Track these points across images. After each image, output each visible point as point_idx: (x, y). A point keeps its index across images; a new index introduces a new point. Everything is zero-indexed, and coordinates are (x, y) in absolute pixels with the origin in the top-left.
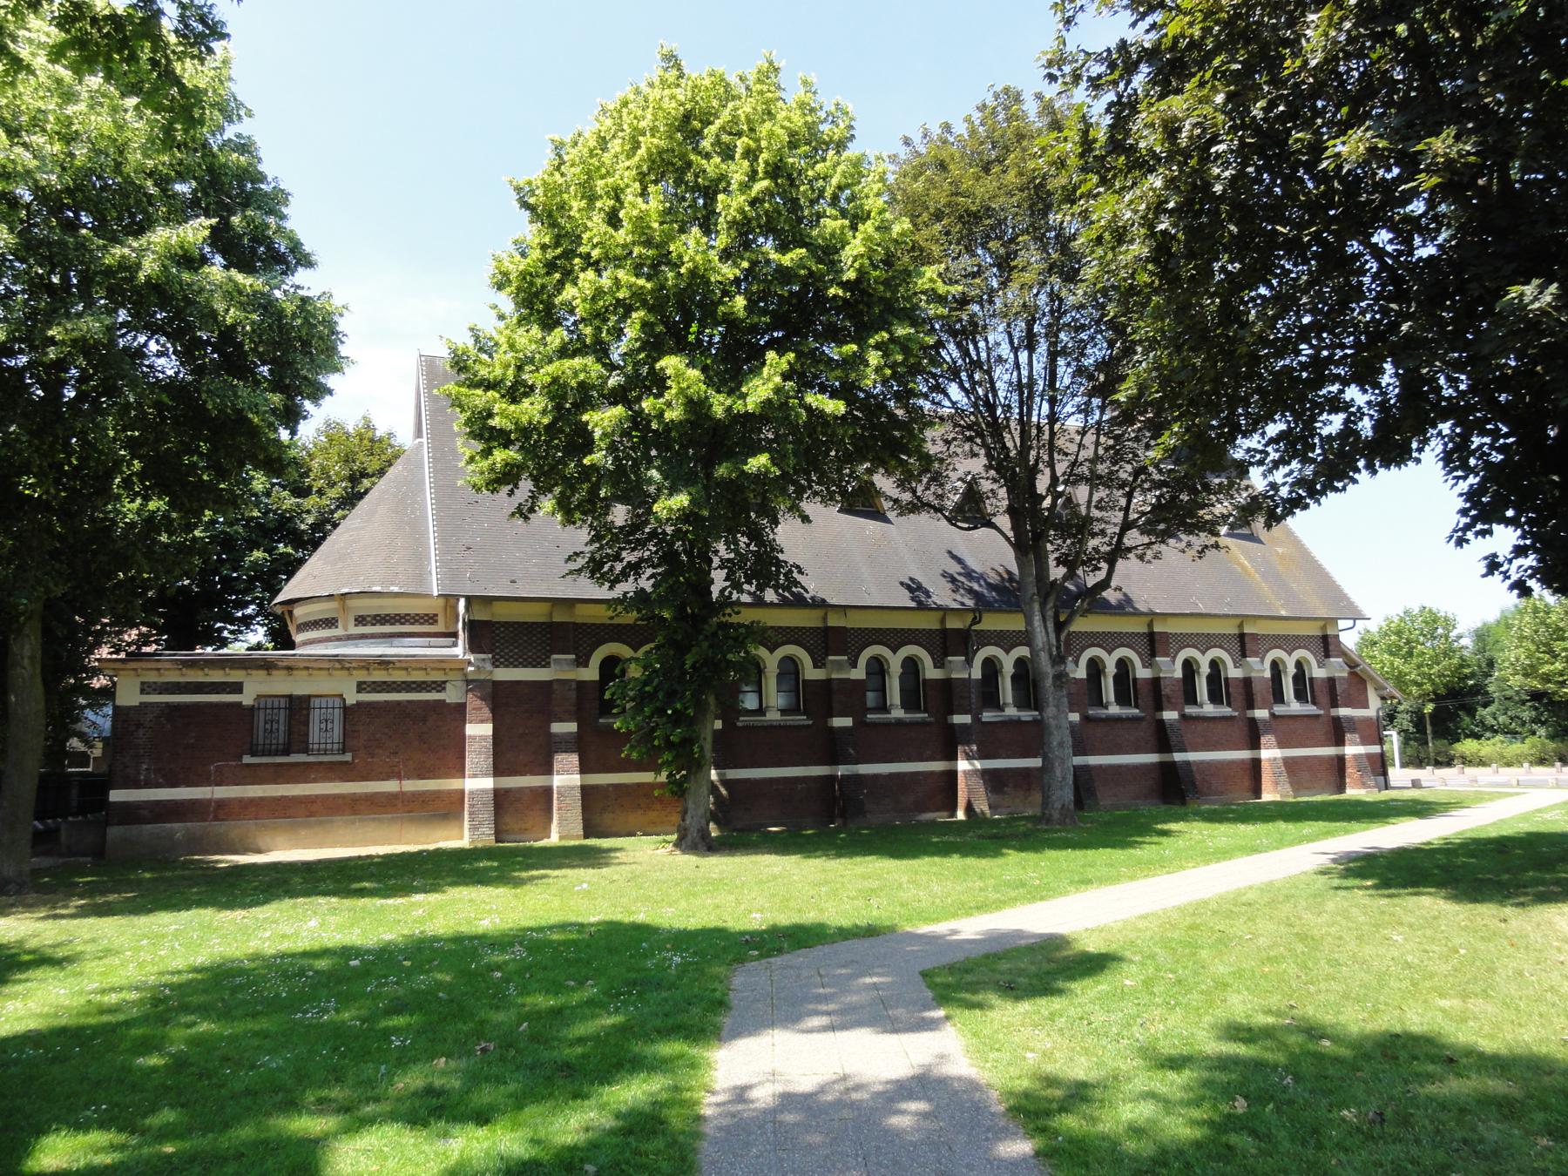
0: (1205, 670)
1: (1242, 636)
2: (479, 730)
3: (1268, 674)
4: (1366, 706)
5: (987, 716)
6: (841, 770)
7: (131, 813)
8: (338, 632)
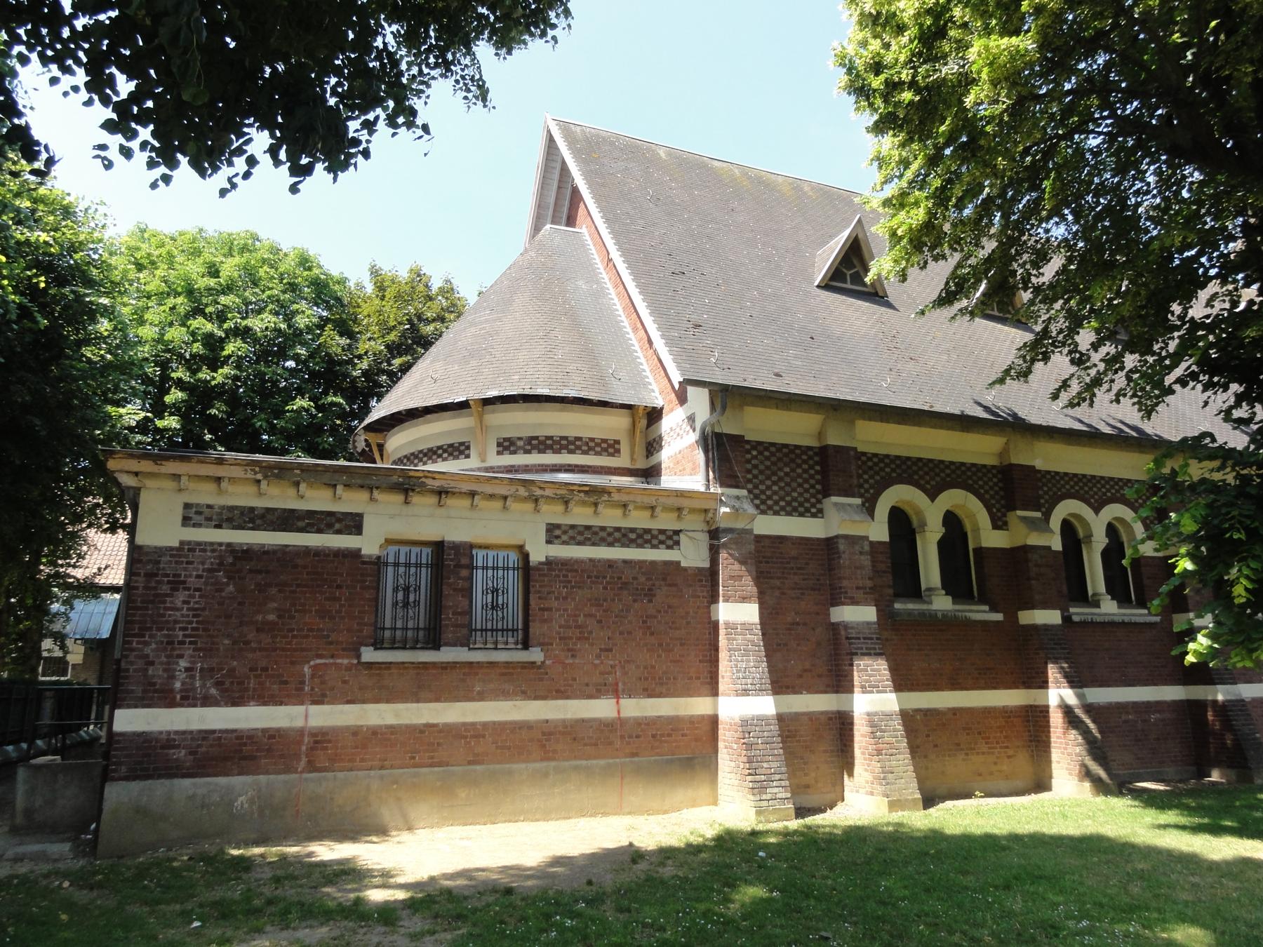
2: (738, 613)
7: (152, 757)
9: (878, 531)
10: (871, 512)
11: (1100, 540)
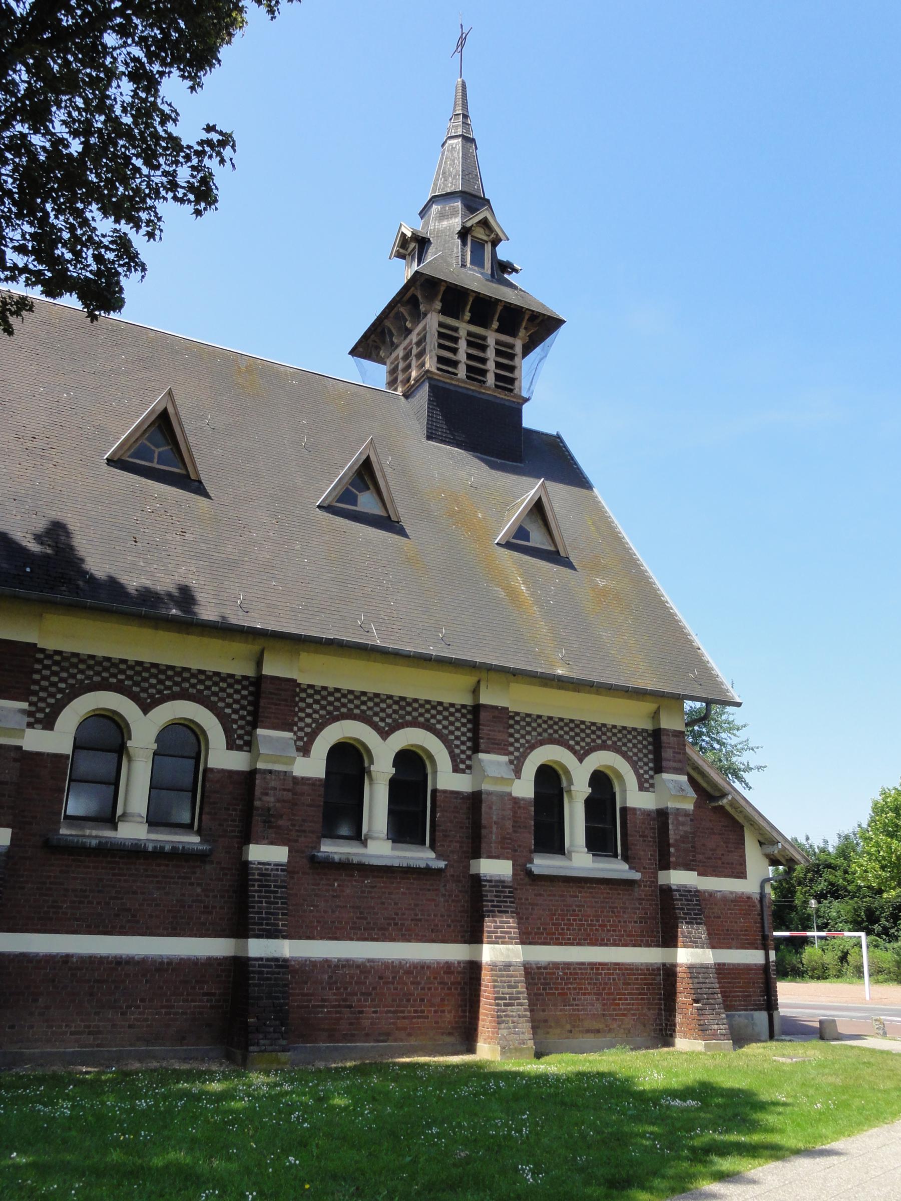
1: (477, 709)
4: (741, 874)
6: (258, 948)
9: (524, 788)
10: (518, 772)
11: (580, 788)
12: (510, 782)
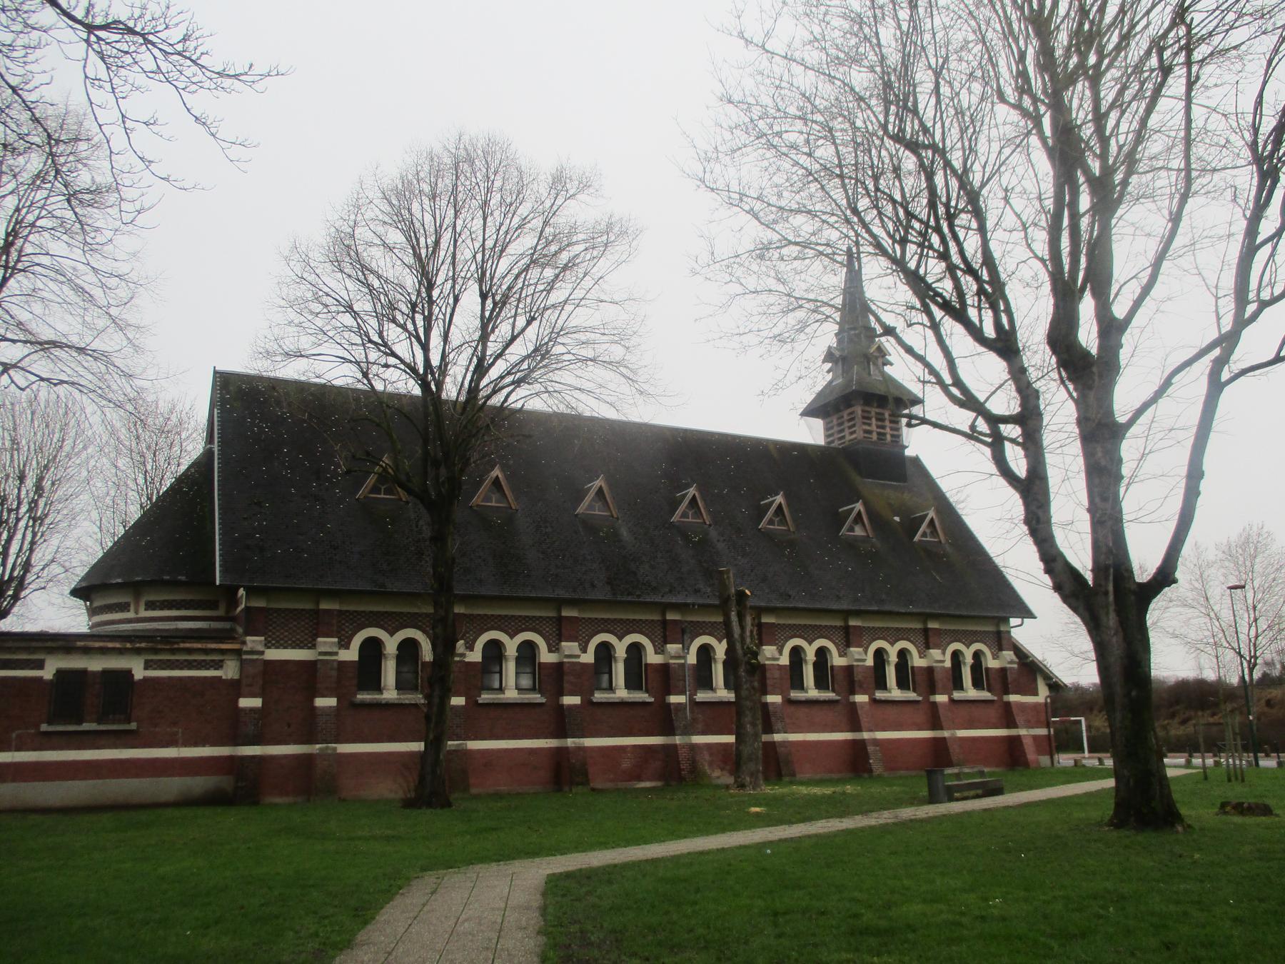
0: (893, 658)
3: (948, 664)
4: (1036, 694)
5: (702, 696)
6: (570, 742)
8: (130, 615)
9: (785, 660)
10: (781, 653)
12: (777, 659)
